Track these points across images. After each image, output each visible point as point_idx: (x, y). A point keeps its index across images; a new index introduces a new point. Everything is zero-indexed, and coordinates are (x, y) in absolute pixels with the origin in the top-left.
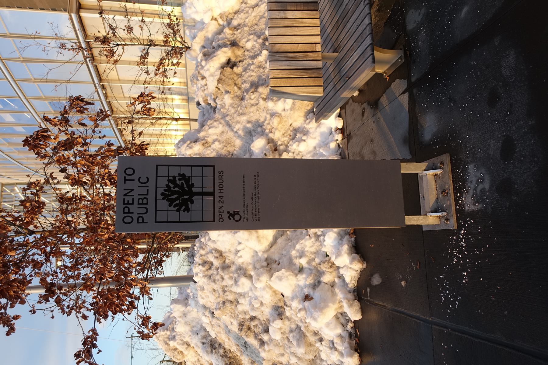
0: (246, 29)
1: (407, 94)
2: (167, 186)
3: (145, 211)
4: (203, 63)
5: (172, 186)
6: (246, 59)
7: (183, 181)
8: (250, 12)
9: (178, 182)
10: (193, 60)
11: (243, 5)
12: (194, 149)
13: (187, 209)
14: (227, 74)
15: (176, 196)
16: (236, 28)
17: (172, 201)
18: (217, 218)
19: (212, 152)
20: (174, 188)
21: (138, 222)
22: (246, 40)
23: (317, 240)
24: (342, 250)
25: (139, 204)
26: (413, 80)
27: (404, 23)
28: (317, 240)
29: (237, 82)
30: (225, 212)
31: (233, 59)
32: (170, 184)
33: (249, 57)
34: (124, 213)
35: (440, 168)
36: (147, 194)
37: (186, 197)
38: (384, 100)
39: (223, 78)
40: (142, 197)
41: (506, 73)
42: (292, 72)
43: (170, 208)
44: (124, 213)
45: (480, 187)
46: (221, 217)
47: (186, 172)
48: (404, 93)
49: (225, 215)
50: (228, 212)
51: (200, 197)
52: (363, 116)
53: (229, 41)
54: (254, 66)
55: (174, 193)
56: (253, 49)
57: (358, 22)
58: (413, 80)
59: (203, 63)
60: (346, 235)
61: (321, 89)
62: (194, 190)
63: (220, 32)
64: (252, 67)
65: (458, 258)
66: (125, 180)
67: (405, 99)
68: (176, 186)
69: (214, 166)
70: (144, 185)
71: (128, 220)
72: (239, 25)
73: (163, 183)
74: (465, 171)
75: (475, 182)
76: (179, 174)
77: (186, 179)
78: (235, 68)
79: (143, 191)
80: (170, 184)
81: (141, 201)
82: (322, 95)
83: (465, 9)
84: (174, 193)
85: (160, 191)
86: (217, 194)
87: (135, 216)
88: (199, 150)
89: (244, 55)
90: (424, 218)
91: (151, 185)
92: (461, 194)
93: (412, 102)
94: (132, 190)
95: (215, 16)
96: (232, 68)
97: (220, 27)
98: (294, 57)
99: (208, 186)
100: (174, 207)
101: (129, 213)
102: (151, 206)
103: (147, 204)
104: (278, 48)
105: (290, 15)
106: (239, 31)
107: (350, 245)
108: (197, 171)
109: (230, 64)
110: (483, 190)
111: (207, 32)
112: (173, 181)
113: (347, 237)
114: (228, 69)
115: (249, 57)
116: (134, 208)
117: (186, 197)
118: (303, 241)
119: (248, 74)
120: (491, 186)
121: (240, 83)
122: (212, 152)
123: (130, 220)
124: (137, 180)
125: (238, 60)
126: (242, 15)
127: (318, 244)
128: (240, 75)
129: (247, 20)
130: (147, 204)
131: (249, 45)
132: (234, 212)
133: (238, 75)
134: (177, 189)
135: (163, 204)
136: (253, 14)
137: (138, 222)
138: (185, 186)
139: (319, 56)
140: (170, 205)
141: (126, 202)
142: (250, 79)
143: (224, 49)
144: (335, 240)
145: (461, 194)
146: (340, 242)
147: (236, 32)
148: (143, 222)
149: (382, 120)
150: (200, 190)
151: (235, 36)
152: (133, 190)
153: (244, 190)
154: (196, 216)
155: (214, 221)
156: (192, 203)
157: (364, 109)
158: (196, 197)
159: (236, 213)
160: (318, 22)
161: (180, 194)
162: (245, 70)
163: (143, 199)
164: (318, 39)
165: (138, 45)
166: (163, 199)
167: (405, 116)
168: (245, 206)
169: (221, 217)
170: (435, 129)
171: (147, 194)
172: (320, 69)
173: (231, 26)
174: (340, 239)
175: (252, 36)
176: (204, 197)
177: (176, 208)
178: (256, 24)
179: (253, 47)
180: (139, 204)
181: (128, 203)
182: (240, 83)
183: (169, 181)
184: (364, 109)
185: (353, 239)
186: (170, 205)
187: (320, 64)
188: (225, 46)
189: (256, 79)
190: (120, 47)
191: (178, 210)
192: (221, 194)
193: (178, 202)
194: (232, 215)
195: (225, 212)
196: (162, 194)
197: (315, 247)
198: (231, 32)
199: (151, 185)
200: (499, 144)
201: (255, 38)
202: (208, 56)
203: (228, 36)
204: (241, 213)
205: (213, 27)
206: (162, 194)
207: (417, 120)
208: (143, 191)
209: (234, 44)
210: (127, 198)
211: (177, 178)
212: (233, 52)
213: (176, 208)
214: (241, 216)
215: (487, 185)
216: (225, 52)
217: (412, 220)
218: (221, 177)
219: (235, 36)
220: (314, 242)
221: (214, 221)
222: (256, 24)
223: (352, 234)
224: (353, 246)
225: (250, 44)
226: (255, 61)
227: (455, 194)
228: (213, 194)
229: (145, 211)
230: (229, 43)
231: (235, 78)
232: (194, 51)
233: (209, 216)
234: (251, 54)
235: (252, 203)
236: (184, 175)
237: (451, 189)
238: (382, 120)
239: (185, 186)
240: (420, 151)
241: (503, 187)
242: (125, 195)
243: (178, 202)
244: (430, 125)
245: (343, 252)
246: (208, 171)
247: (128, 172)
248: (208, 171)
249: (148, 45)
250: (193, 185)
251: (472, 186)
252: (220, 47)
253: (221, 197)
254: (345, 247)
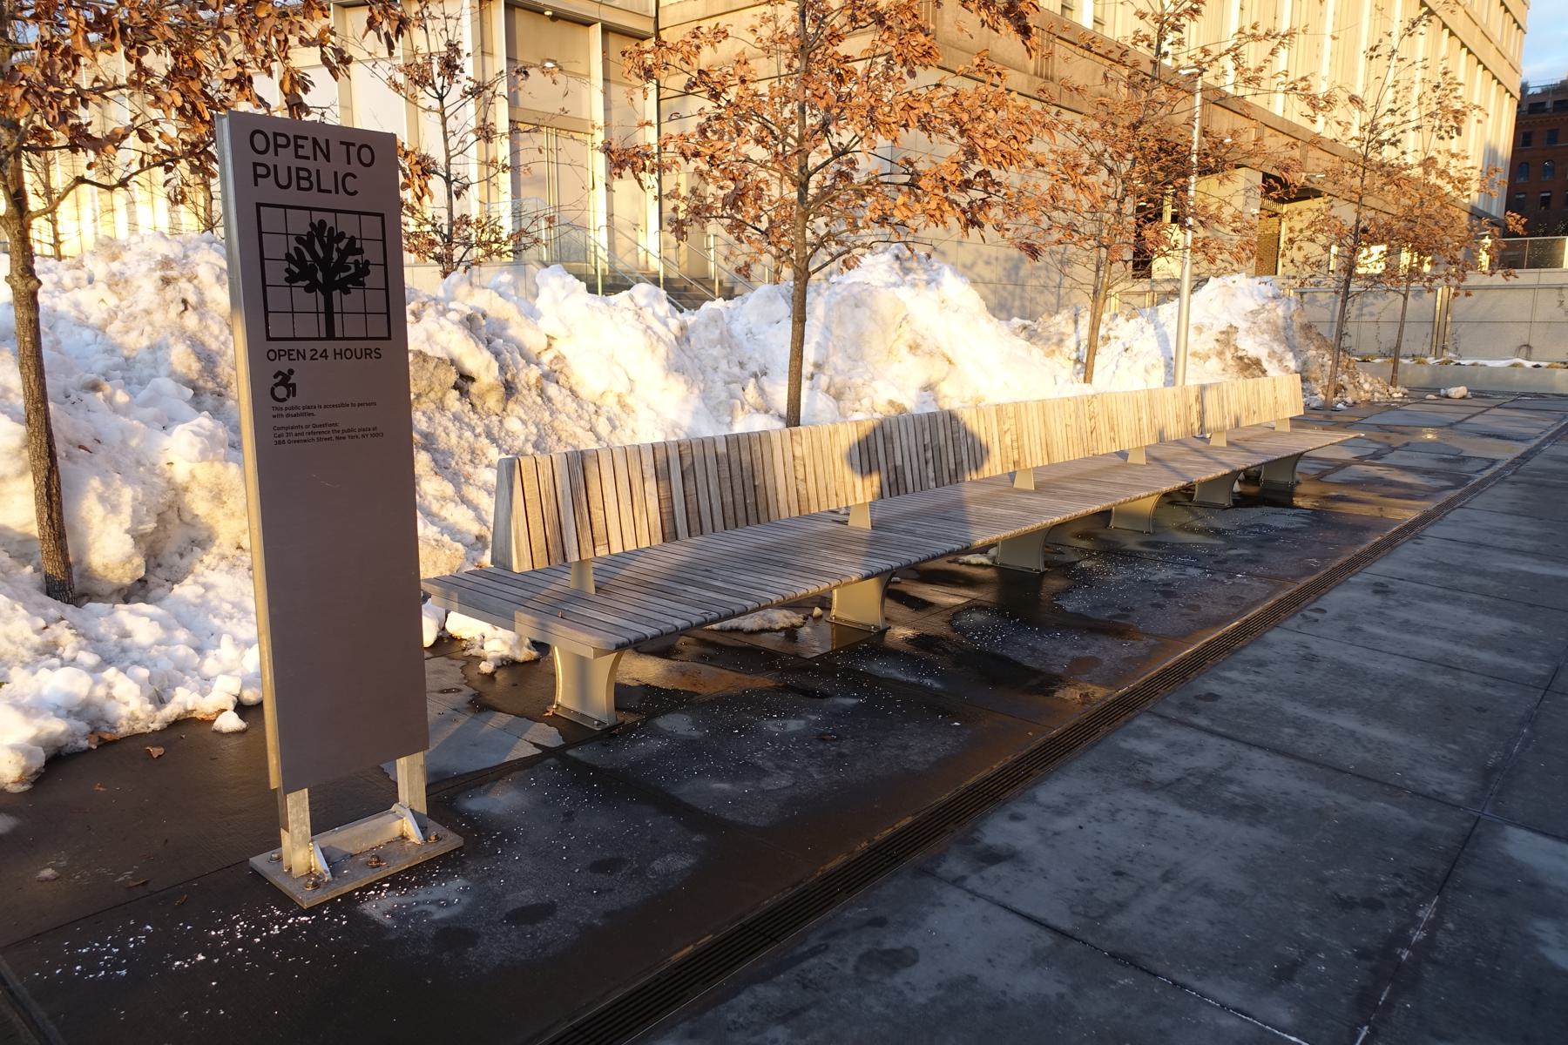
0: (546, 416)
1: (539, 751)
2: (342, 236)
3: (284, 182)
4: (453, 316)
5: (342, 245)
6: (481, 418)
7: (353, 270)
8: (582, 423)
9: (351, 259)
10: (446, 291)
11: (592, 408)
12: (217, 288)
13: (292, 279)
14: (441, 373)
15: (321, 254)
16: (542, 393)
17: (309, 245)
18: (276, 345)
19: (217, 338)
20: (338, 250)
21: (255, 165)
22: (524, 417)
23: (36, 650)
24: (47, 719)
25: (298, 169)
26: (571, 752)
27: (664, 713)
28: (36, 650)
29: (423, 399)
30: (291, 365)
31: (474, 388)
32: (345, 241)
33: (487, 426)
34: (276, 135)
35: (426, 839)
36: (320, 190)
37: (320, 276)
38: (500, 719)
39: (431, 366)
40: (314, 178)
41: (657, 865)
42: (553, 501)
43: (292, 239)
44: (276, 135)
45: (432, 908)
46: (279, 354)
47: (374, 278)
48: (536, 745)
49: (284, 365)
50: (291, 372)
51: (322, 308)
52: (442, 692)
53: (514, 376)
54: (472, 439)
55: (327, 248)
56: (507, 433)
57: (669, 612)
58: (571, 752)
59: (453, 316)
60: (90, 723)
61: (527, 567)
62: (336, 294)
63: (530, 359)
64: (468, 434)
65: (230, 935)
66: (348, 145)
67: (524, 750)
68: (344, 254)
69: (389, 338)
70: (341, 183)
71: (260, 142)
72: (550, 400)
73: (347, 225)
74: (444, 877)
75: (432, 897)
76: (367, 263)
77: (358, 278)
78: (456, 393)
79: (327, 182)
80: (345, 241)
81: (303, 174)
82: (516, 569)
83: (726, 786)
84: (327, 248)
85: (329, 219)
86: (330, 346)
87: (268, 159)
88: (214, 301)
89: (488, 416)
90: (304, 837)
91: (341, 201)
92: (389, 889)
93: (526, 763)
94: (327, 158)
95: (555, 343)
96: (456, 387)
97: (533, 355)
98: (580, 504)
99: (349, 325)
100: (296, 249)
101: (277, 146)
102: (292, 196)
103: (299, 188)
104: (592, 469)
105: (651, 485)
106: (539, 400)
107: (64, 740)
108: (376, 301)
109: (464, 380)
110: (428, 914)
111: (519, 324)
112: (352, 249)
113: (84, 727)
114: (453, 377)
115: (487, 426)
116: (286, 158)
117: (320, 276)
118: (21, 611)
119: (450, 425)
120: (442, 920)
121: (424, 407)
122: (217, 338)
123: (261, 147)
124: (350, 169)
125: (475, 401)
126: (571, 406)
127: (27, 655)
128: (442, 407)
129: (563, 417)
130: (299, 188)
131: (513, 424)
132: (294, 385)
133: (441, 400)
134: (335, 256)
135: (300, 224)
136: (579, 431)
137: (255, 165)
138: (343, 275)
139: (588, 554)
140: (299, 239)
141: (300, 142)
142: (440, 431)
143: (495, 365)
144: (68, 695)
145: (389, 889)
146: (63, 712)
147: (534, 392)
148: (256, 176)
149: (456, 726)
150: (336, 308)
151: (525, 392)
152: (328, 160)
153: (343, 405)
154: (278, 297)
155: (269, 339)
156: (308, 289)
157: (459, 690)
158: (321, 297)
159: (292, 390)
160: (644, 544)
161: (324, 263)
162: (456, 418)
163: (308, 179)
164: (616, 549)
165: (447, 151)
166: (312, 225)
167: (492, 760)
168: (308, 411)
169: (279, 354)
170: (497, 811)
171: (320, 190)
172: (565, 560)
173: (544, 381)
174: (69, 712)
175: (534, 430)
176: (322, 317)
177: (292, 252)
178: (559, 439)
179: (513, 435)
180: (298, 169)
181: (297, 146)
182: (424, 407)
183: (353, 239)
184: (459, 690)
185: (84, 744)
186: (299, 239)
187: (573, 557)
188: (503, 368)
189: (442, 446)
190: (436, 104)
191: (288, 257)
192: (330, 353)
193: (308, 257)
194: (284, 379)
195: (291, 365)
196: (323, 223)
197: (11, 648)
198: (533, 381)
199: (341, 201)
200: (533, 901)
201: (533, 438)
202: (470, 323)
203: (522, 375)
204: (291, 402)
205: (532, 339)
206: (323, 223)
207: (497, 780)
208: (327, 182)
209: (509, 389)
210: (308, 144)
211: (358, 257)
212: (491, 389)
213: (292, 252)
214: (284, 400)
215: (440, 914)
216: (488, 368)
217: (297, 808)
218: (367, 353)
219: (525, 392)
220: (28, 645)
221: (269, 339)
222: (559, 439)
223: (101, 739)
224: (60, 749)
225: (517, 426)
226: (484, 441)
227: (384, 880)
228: (331, 336)
229: (283, 181)
230: (509, 376)
231: (432, 395)
232: (470, 294)
233: (279, 327)
234: (495, 431)
235: (315, 426)
236: (368, 273)
237: (392, 870)
238: (456, 726)
239: (343, 275)
240: (444, 798)
241: (455, 935)
242: (315, 141)
243: (308, 257)
244: (501, 801)
245: (39, 722)
246: (377, 327)
247: (365, 153)
248: (377, 327)
249: (449, 174)
250: (347, 292)
251: (422, 896)
252: (497, 355)
253: (324, 355)
254: (57, 726)
